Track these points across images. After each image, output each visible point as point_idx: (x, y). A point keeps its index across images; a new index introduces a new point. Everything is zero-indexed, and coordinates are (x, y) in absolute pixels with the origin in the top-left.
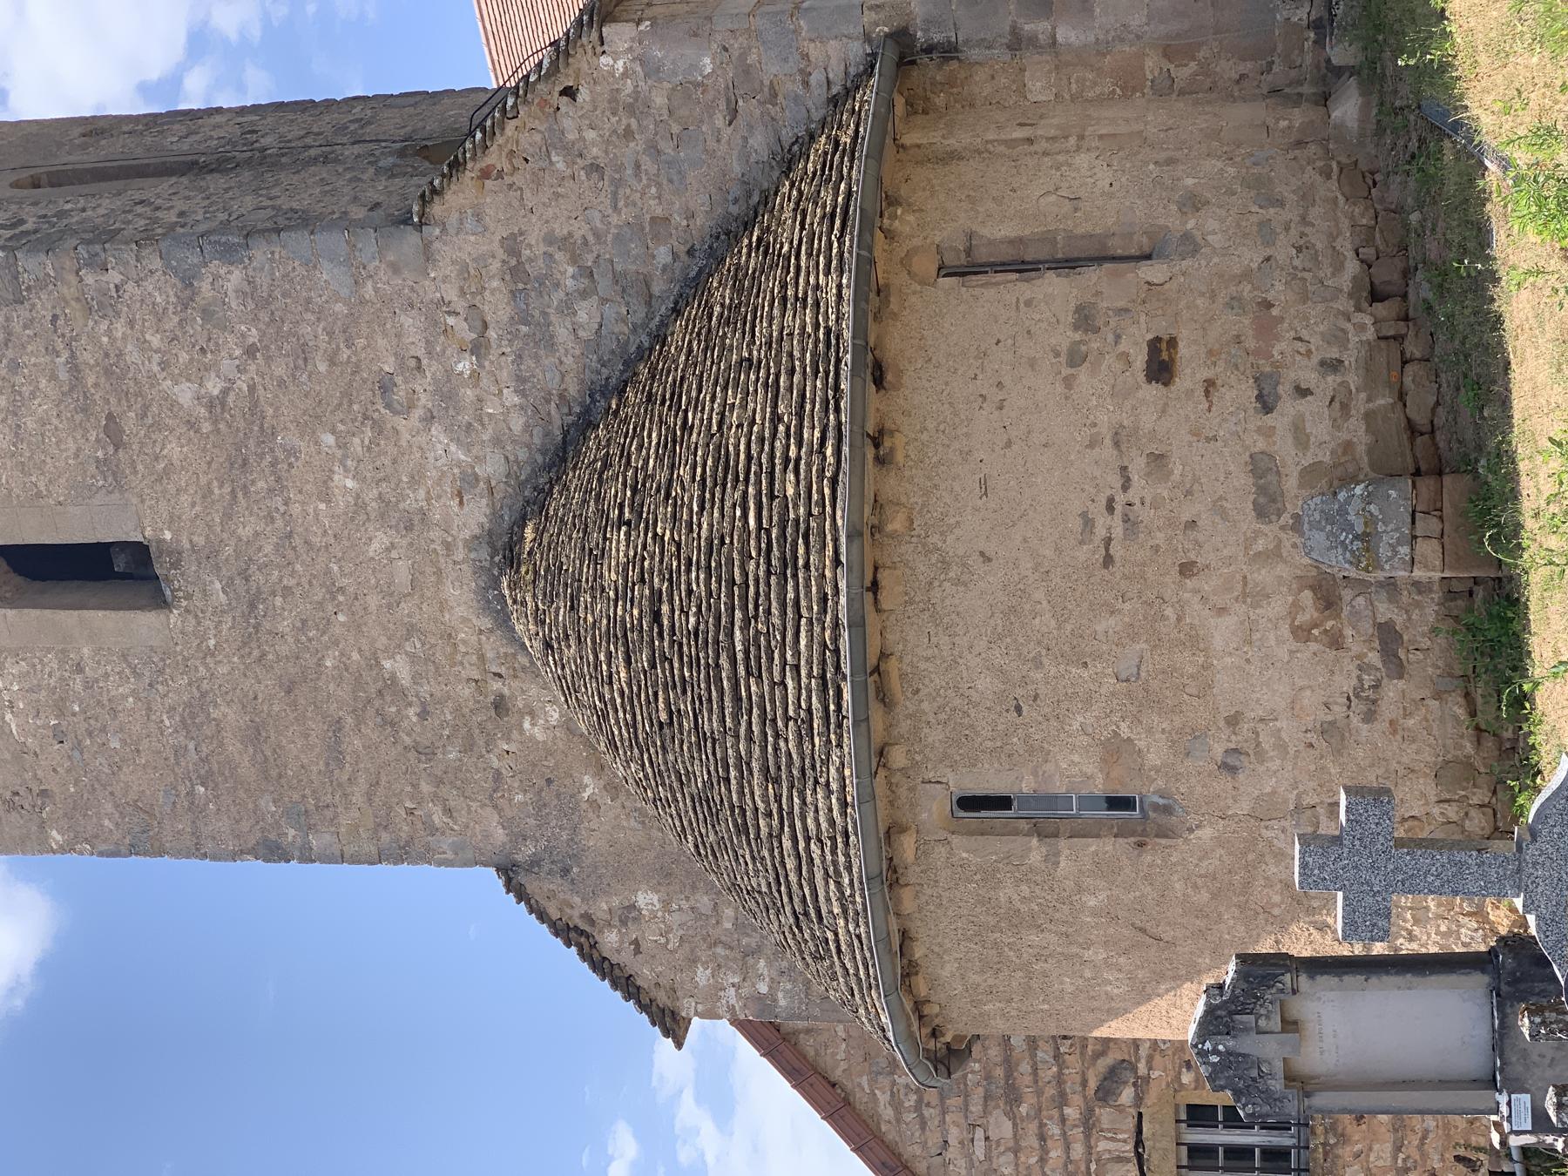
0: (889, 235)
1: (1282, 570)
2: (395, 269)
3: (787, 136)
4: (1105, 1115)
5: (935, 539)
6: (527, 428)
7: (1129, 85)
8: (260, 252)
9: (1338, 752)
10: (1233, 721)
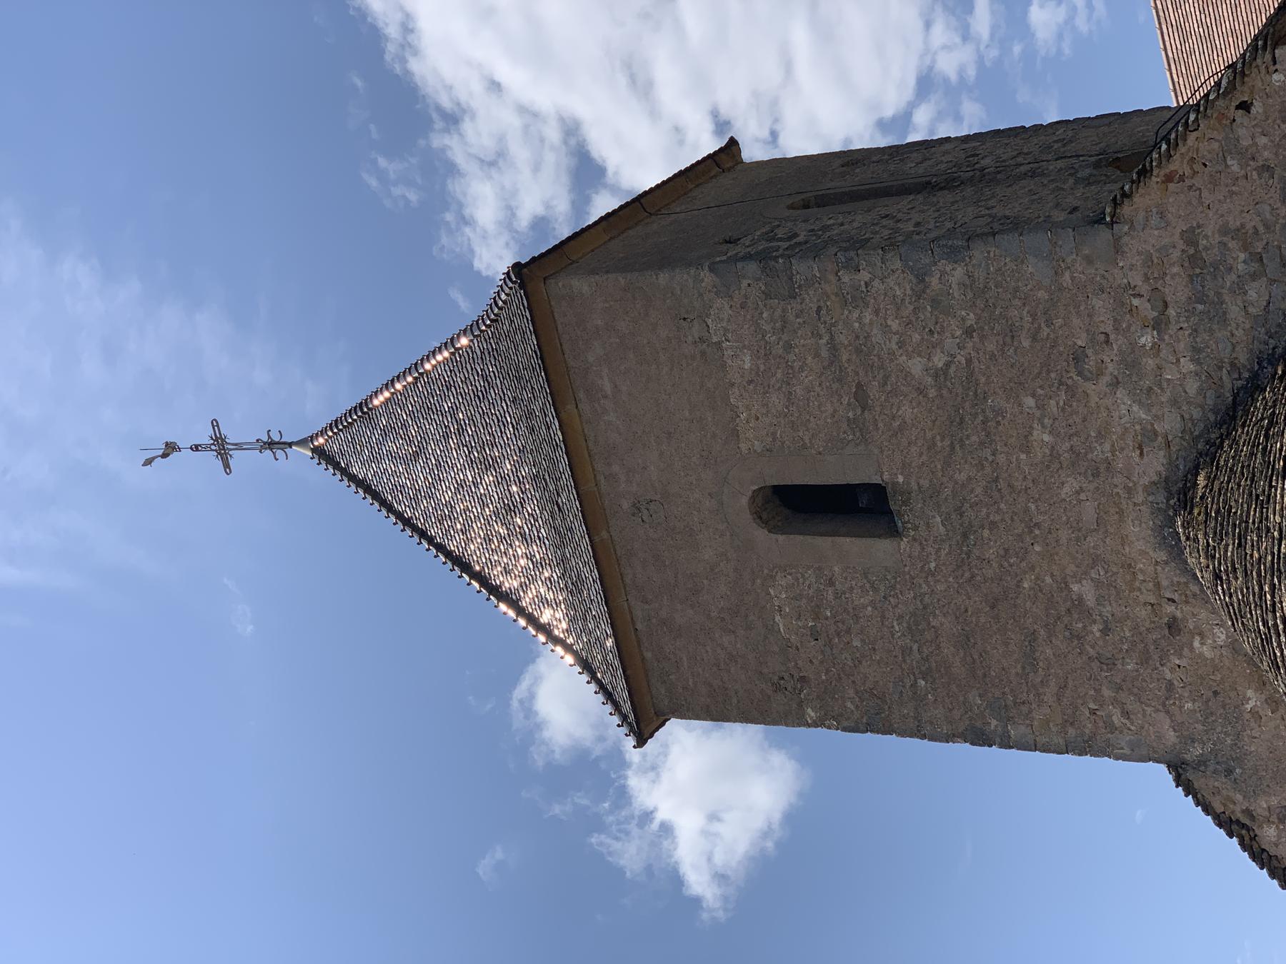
2: (1089, 260)
6: (1201, 391)
8: (978, 252)
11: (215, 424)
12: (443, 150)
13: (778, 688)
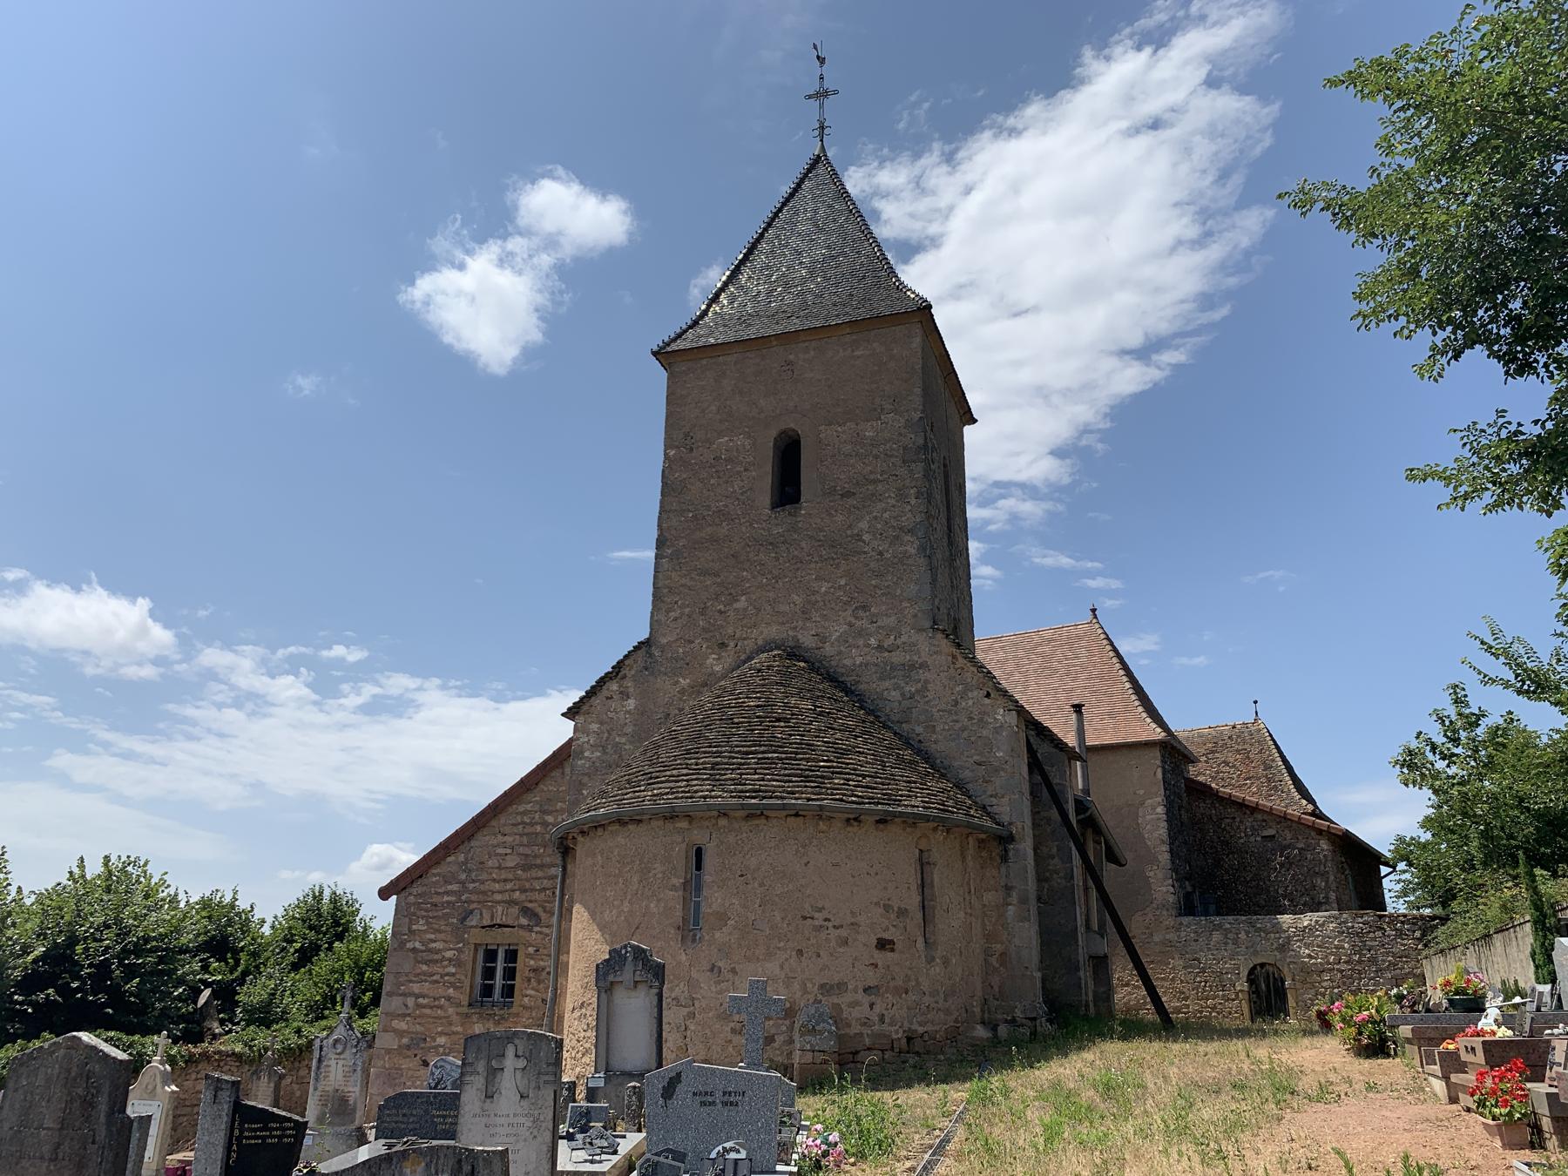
0: (935, 829)
1: (799, 994)
2: (915, 616)
3: (969, 786)
4: (515, 910)
5: (815, 842)
6: (845, 666)
7: (989, 937)
8: (922, 561)
9: (718, 1017)
10: (733, 971)
11: (836, 92)
12: (931, 150)
13: (686, 435)
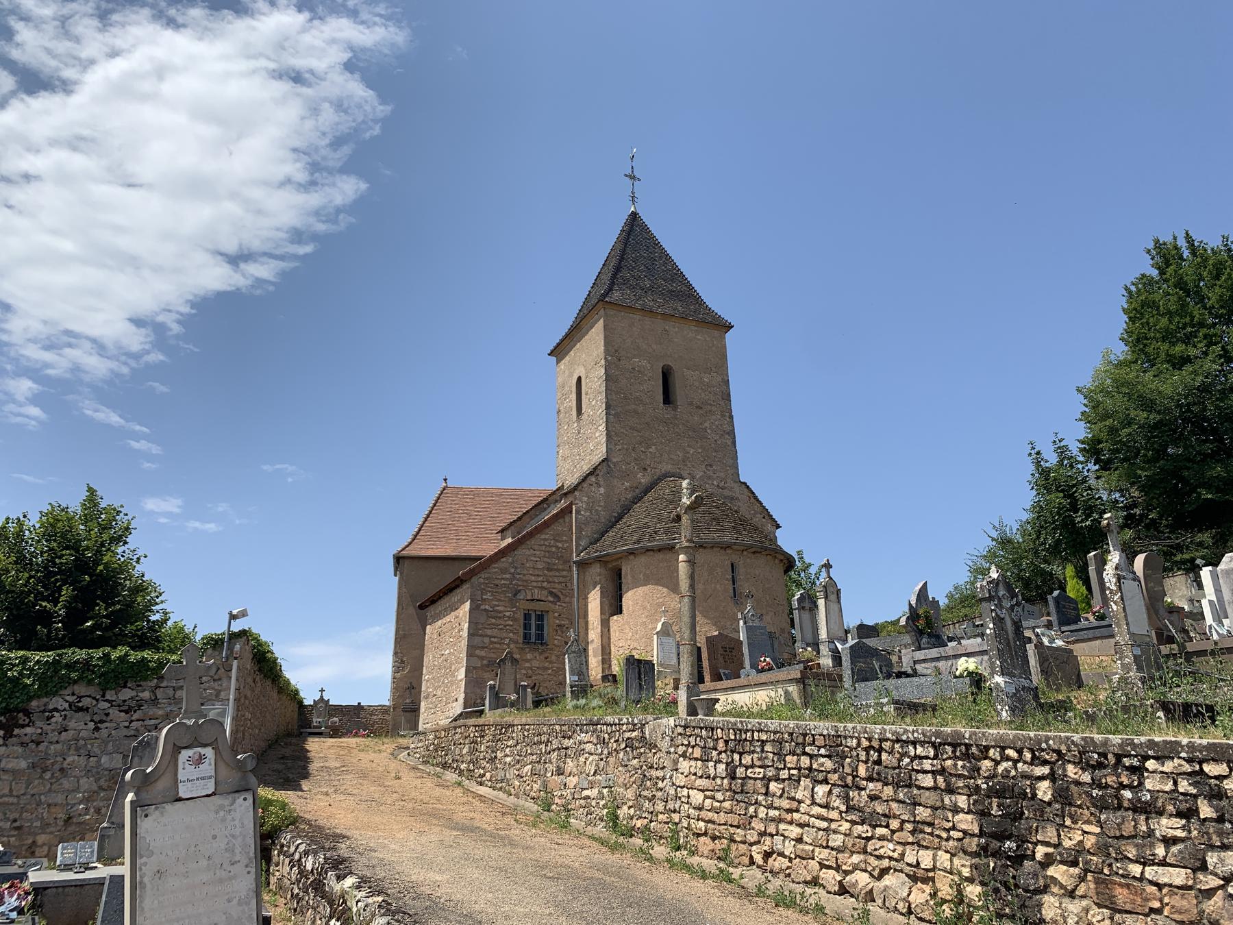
4: (545, 593)
